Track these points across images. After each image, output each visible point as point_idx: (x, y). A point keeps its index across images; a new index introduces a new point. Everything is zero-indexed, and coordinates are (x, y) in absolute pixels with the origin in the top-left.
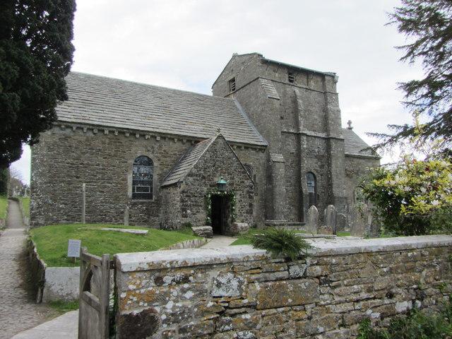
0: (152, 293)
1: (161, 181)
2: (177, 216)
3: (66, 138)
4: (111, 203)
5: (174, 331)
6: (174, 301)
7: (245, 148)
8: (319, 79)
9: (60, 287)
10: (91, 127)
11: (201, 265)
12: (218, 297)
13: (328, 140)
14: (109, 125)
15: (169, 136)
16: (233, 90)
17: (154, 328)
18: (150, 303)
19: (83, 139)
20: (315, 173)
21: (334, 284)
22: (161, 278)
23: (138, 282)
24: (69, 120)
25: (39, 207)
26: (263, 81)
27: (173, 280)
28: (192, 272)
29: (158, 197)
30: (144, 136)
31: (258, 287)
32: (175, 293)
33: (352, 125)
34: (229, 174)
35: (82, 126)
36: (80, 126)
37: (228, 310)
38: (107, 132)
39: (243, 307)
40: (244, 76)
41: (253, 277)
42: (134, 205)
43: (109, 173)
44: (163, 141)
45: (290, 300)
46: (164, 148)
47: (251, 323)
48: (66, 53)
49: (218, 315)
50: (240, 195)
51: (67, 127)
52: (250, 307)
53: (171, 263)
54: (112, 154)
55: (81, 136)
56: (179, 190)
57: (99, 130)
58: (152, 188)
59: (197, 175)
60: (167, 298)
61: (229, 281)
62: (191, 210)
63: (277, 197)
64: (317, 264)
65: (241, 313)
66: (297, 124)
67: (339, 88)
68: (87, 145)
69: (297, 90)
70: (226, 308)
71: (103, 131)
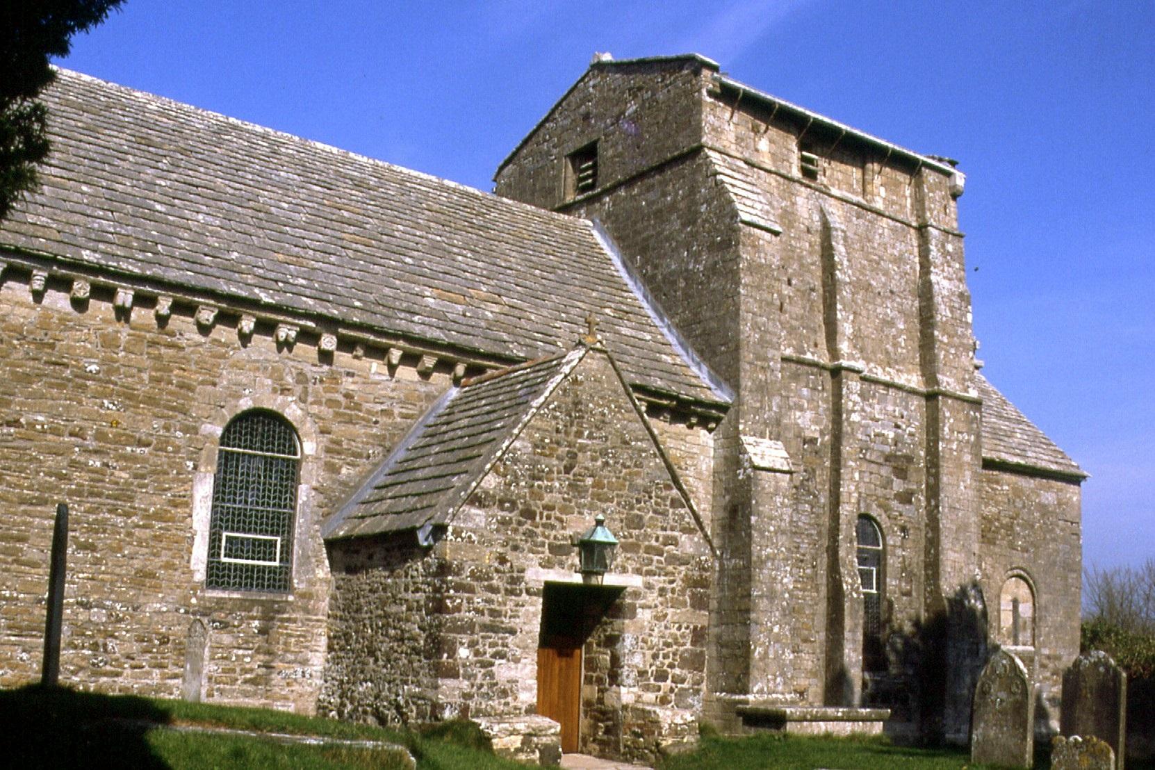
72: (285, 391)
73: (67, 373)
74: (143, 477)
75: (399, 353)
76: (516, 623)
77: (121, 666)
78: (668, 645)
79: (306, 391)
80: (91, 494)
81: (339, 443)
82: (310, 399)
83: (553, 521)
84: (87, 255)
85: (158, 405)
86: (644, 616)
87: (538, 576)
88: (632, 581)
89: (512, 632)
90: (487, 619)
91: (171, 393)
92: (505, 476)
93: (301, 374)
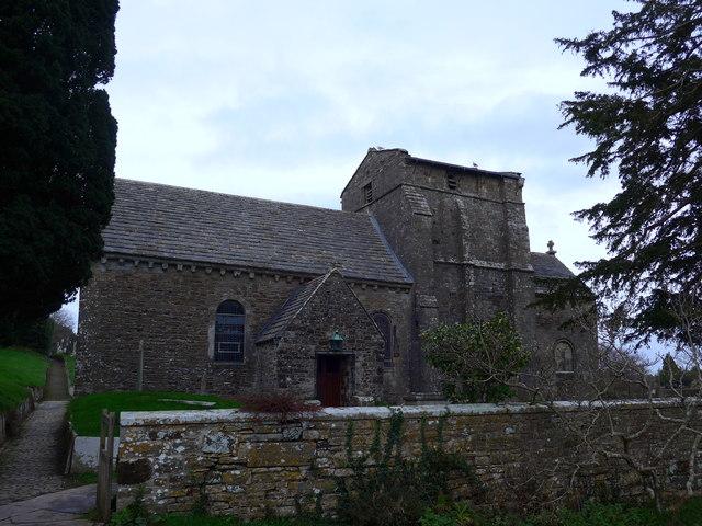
0: (147, 445)
1: (256, 336)
3: (126, 276)
7: (380, 287)
8: (495, 183)
13: (508, 272)
14: (182, 257)
18: (145, 454)
19: (147, 276)
21: (333, 448)
22: (156, 433)
24: (131, 252)
26: (407, 190)
27: (166, 436)
30: (232, 272)
33: (554, 248)
36: (144, 260)
38: (180, 267)
40: (387, 177)
44: (259, 279)
45: (283, 461)
46: (260, 289)
48: (110, 160)
51: (127, 261)
52: (241, 464)
53: (165, 420)
55: (145, 273)
56: (276, 349)
58: (242, 345)
61: (219, 439)
62: (292, 378)
64: (314, 428)
66: (461, 250)
67: (527, 195)
69: (460, 201)
70: (216, 463)
71: (175, 266)
84: (166, 255)
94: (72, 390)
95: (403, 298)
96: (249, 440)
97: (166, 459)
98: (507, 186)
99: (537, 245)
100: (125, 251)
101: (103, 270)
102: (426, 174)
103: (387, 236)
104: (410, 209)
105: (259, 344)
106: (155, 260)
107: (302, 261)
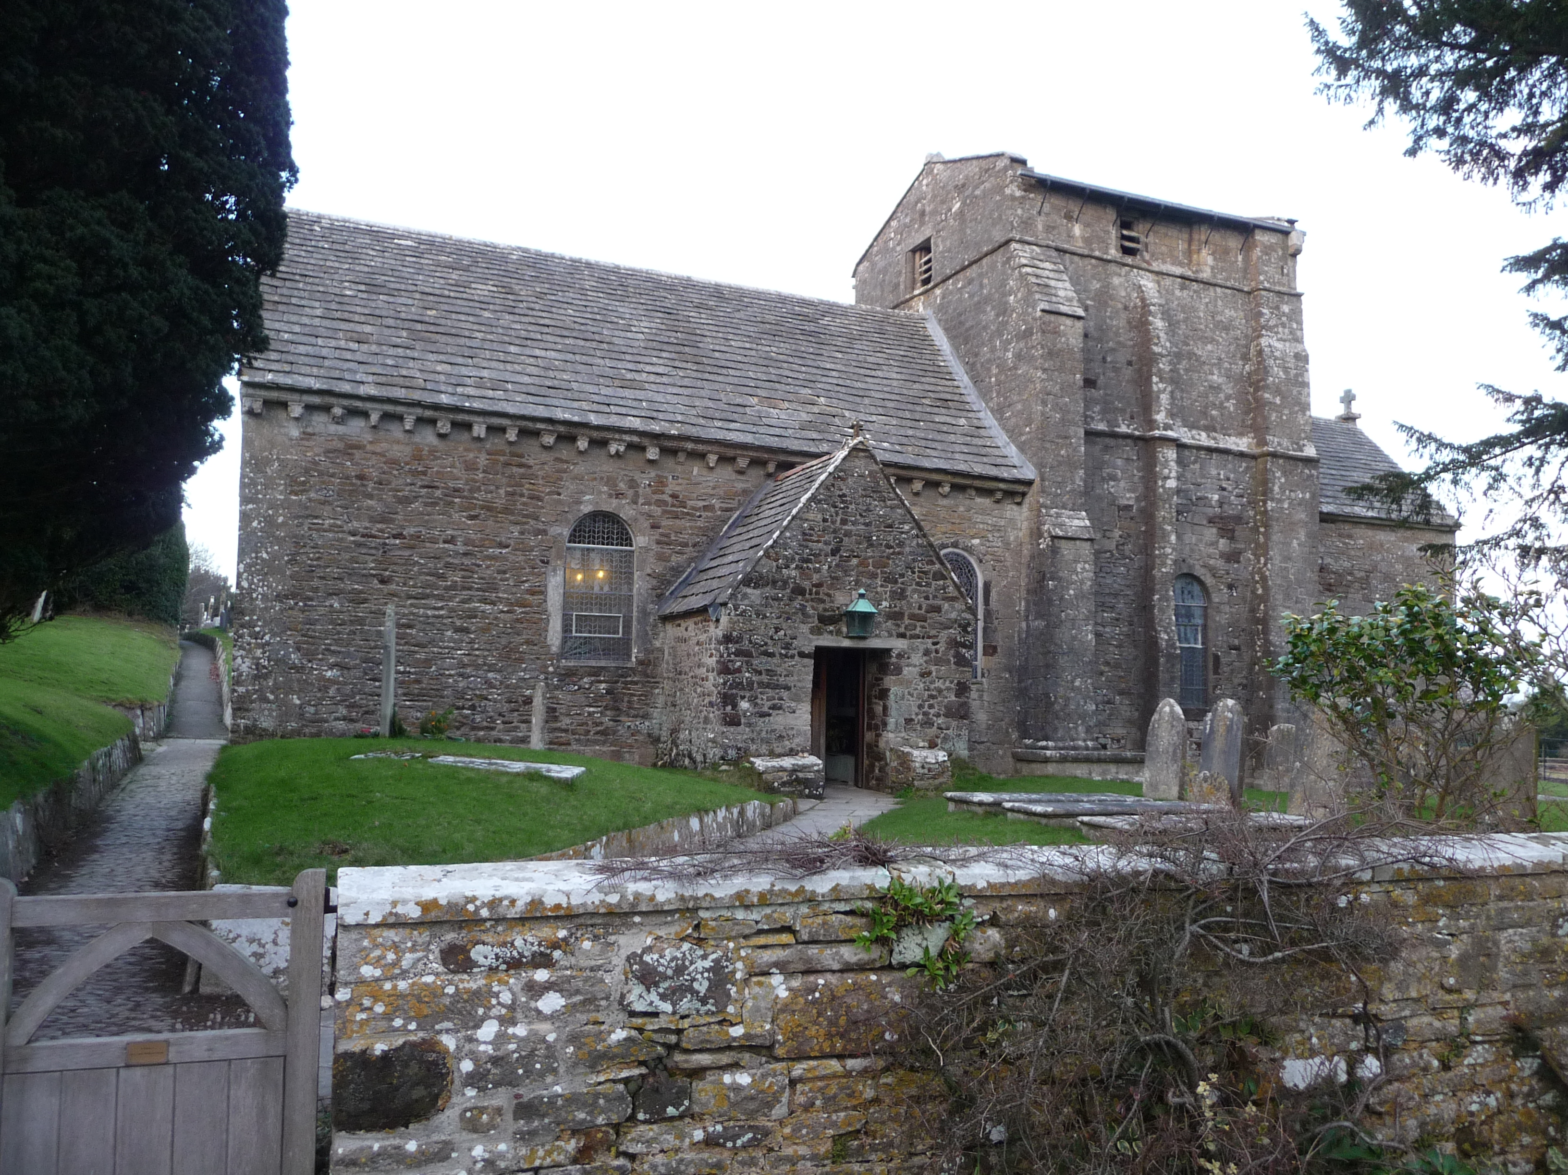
0: (435, 992)
2: (707, 720)
3: (350, 448)
4: (492, 668)
5: (499, 1111)
6: (502, 1020)
7: (955, 487)
8: (1233, 242)
9: (255, 947)
10: (428, 413)
11: (593, 914)
12: (645, 1014)
15: (690, 446)
16: (926, 282)
17: (437, 1097)
19: (401, 452)
20: (1209, 581)
23: (391, 956)
25: (259, 675)
26: (1023, 254)
28: (562, 934)
29: (648, 651)
31: (780, 987)
32: (506, 997)
34: (890, 579)
35: (400, 409)
37: (678, 1057)
38: (479, 430)
39: (729, 1048)
40: (982, 220)
41: (767, 956)
42: (568, 675)
43: (488, 570)
44: (669, 462)
46: (672, 486)
47: (752, 1098)
49: (643, 1070)
50: (927, 653)
53: (494, 903)
54: (500, 503)
55: (397, 442)
57: (454, 424)
59: (774, 582)
60: (481, 1011)
62: (753, 700)
63: (1063, 661)
65: (720, 1068)
66: (1146, 405)
67: (1307, 275)
68: (415, 473)
69: (1148, 284)
70: (670, 1048)
71: (468, 426)
72: (619, 495)
73: (438, 493)
74: (505, 572)
75: (715, 457)
76: (791, 681)
77: (494, 722)
78: (932, 697)
79: (637, 495)
80: (464, 588)
81: (667, 536)
82: (641, 501)
83: (821, 596)
84: (444, 399)
85: (513, 514)
86: (908, 672)
87: (810, 642)
88: (899, 645)
89: (787, 688)
90: (765, 678)
91: (524, 504)
92: (777, 560)
93: (632, 480)
94: (228, 719)
95: (1008, 514)
96: (782, 967)
97: (500, 1039)
98: (1254, 246)
99: (1324, 406)
100: (346, 388)
101: (295, 432)
102: (1069, 217)
103: (971, 368)
104: (1028, 301)
105: (667, 619)
106: (419, 411)
107: (779, 422)
